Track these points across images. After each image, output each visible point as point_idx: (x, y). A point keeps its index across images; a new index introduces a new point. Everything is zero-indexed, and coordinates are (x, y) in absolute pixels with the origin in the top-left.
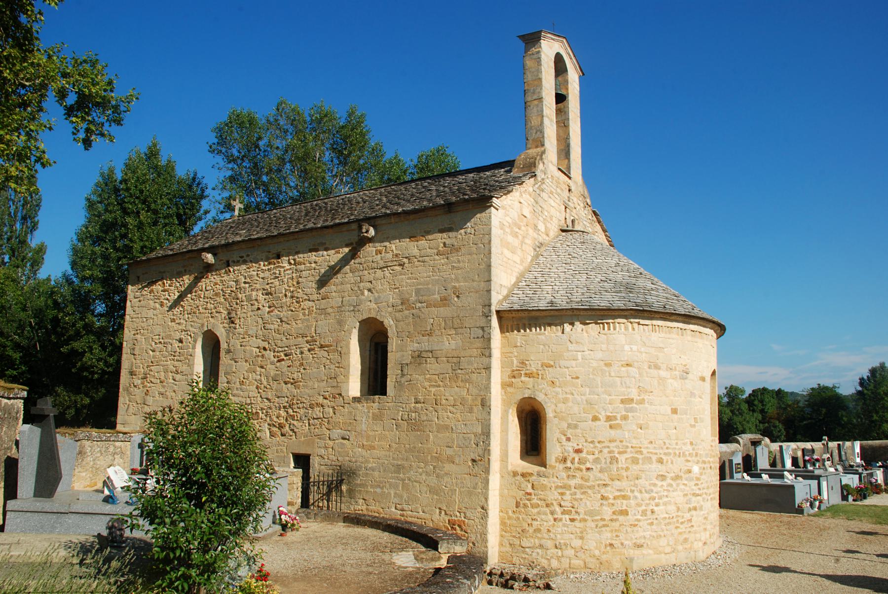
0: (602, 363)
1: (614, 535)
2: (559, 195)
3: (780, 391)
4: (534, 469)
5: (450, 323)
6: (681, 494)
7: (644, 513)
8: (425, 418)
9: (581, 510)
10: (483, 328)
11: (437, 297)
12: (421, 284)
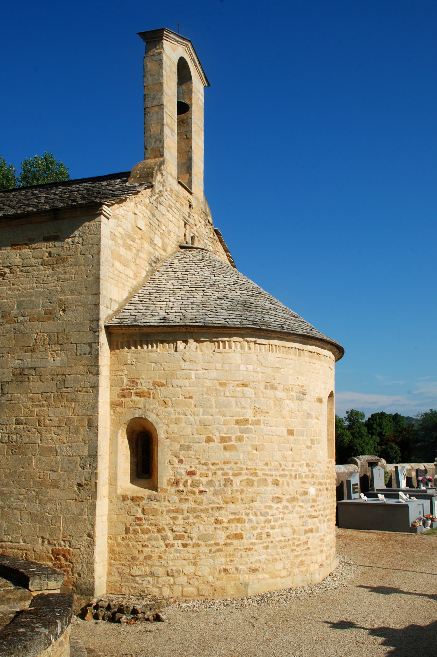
0: (217, 383)
1: (228, 560)
2: (178, 209)
3: (396, 415)
4: (145, 492)
5: (54, 338)
7: (259, 536)
8: (27, 440)
9: (194, 535)
10: (90, 344)
11: (41, 309)
12: (23, 296)
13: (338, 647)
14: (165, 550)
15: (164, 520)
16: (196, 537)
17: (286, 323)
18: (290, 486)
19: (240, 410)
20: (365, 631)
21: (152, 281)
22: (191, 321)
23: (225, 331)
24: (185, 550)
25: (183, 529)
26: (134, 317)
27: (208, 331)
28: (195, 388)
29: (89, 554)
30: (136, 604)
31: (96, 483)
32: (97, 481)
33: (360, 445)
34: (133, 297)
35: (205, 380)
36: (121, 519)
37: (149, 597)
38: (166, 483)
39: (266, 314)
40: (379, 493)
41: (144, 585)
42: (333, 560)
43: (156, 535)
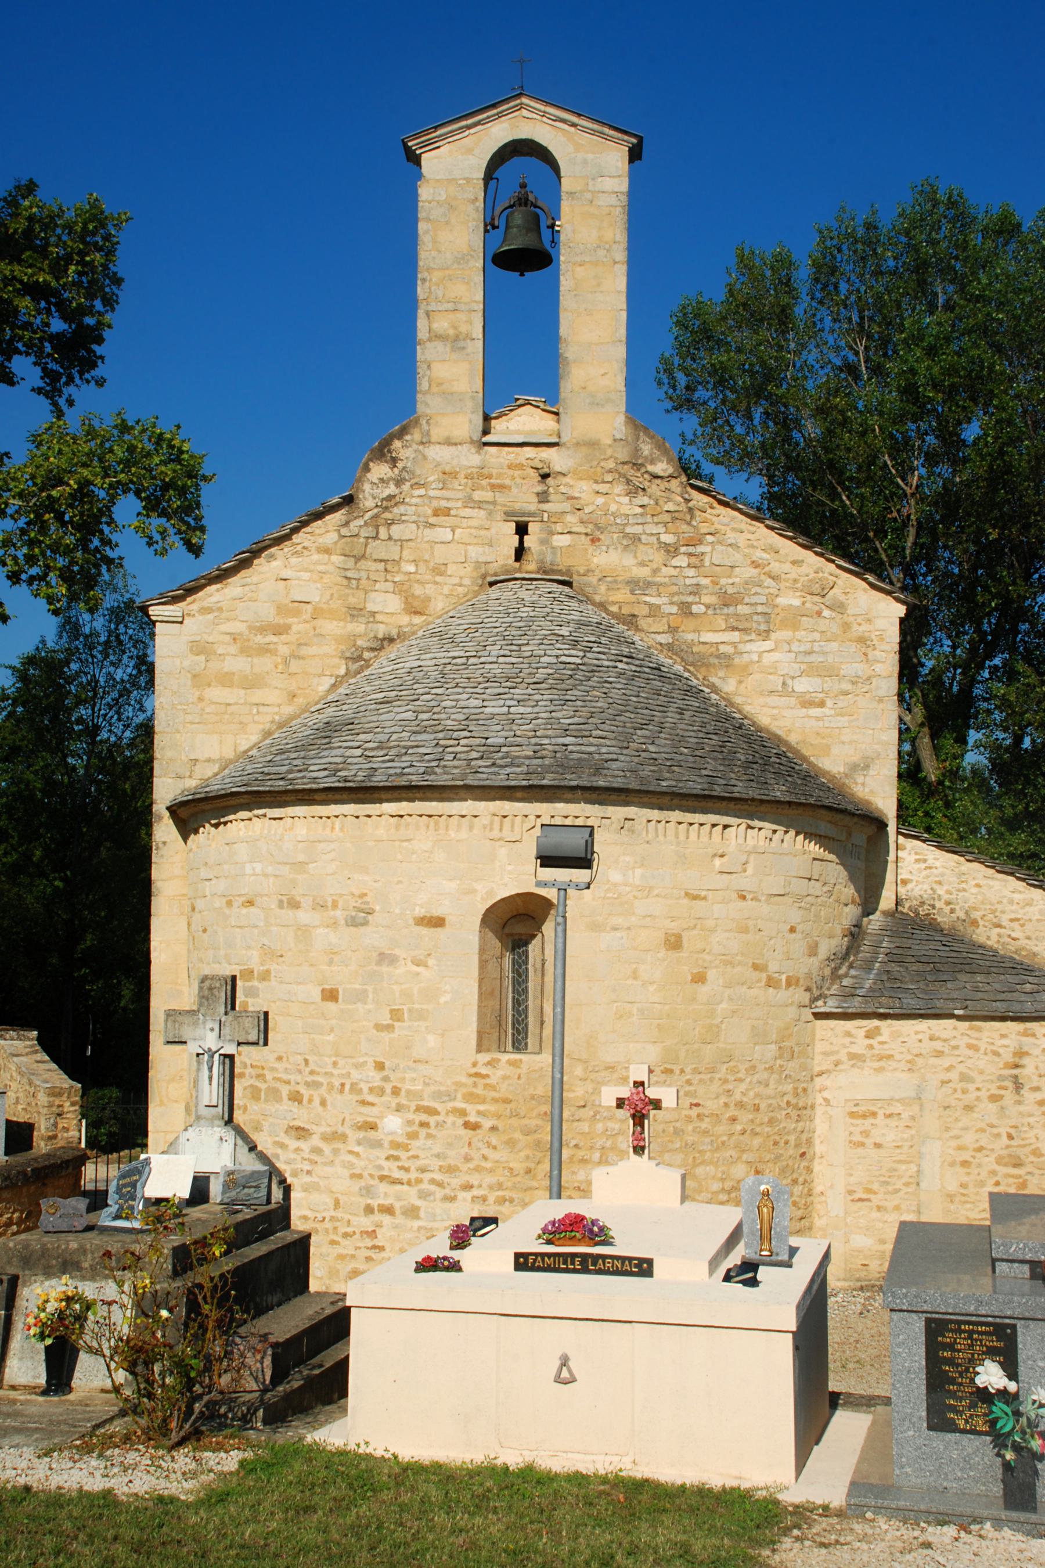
6: (346, 1173)
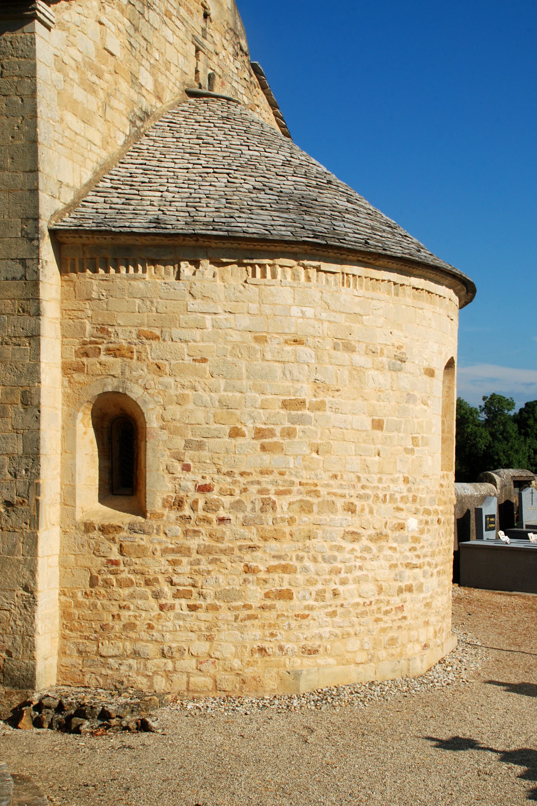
0: (250, 336)
1: (267, 633)
2: (183, 21)
6: (387, 564)
7: (320, 596)
9: (209, 591)
10: (23, 261)
13: (448, 779)
14: (159, 614)
15: (158, 564)
16: (213, 594)
17: (374, 236)
18: (375, 514)
19: (291, 384)
20: (495, 754)
21: (137, 154)
22: (204, 228)
23: (265, 248)
24: (192, 616)
25: (190, 581)
26: (103, 216)
27: (235, 245)
28: (212, 344)
29: (25, 620)
30: (108, 703)
31: (37, 501)
32: (40, 498)
33: (504, 452)
34: (102, 181)
35: (230, 330)
36: (83, 561)
37: (131, 692)
38: (160, 504)
39: (339, 221)
40: (530, 532)
41: (122, 671)
42: (447, 638)
43: (143, 589)
